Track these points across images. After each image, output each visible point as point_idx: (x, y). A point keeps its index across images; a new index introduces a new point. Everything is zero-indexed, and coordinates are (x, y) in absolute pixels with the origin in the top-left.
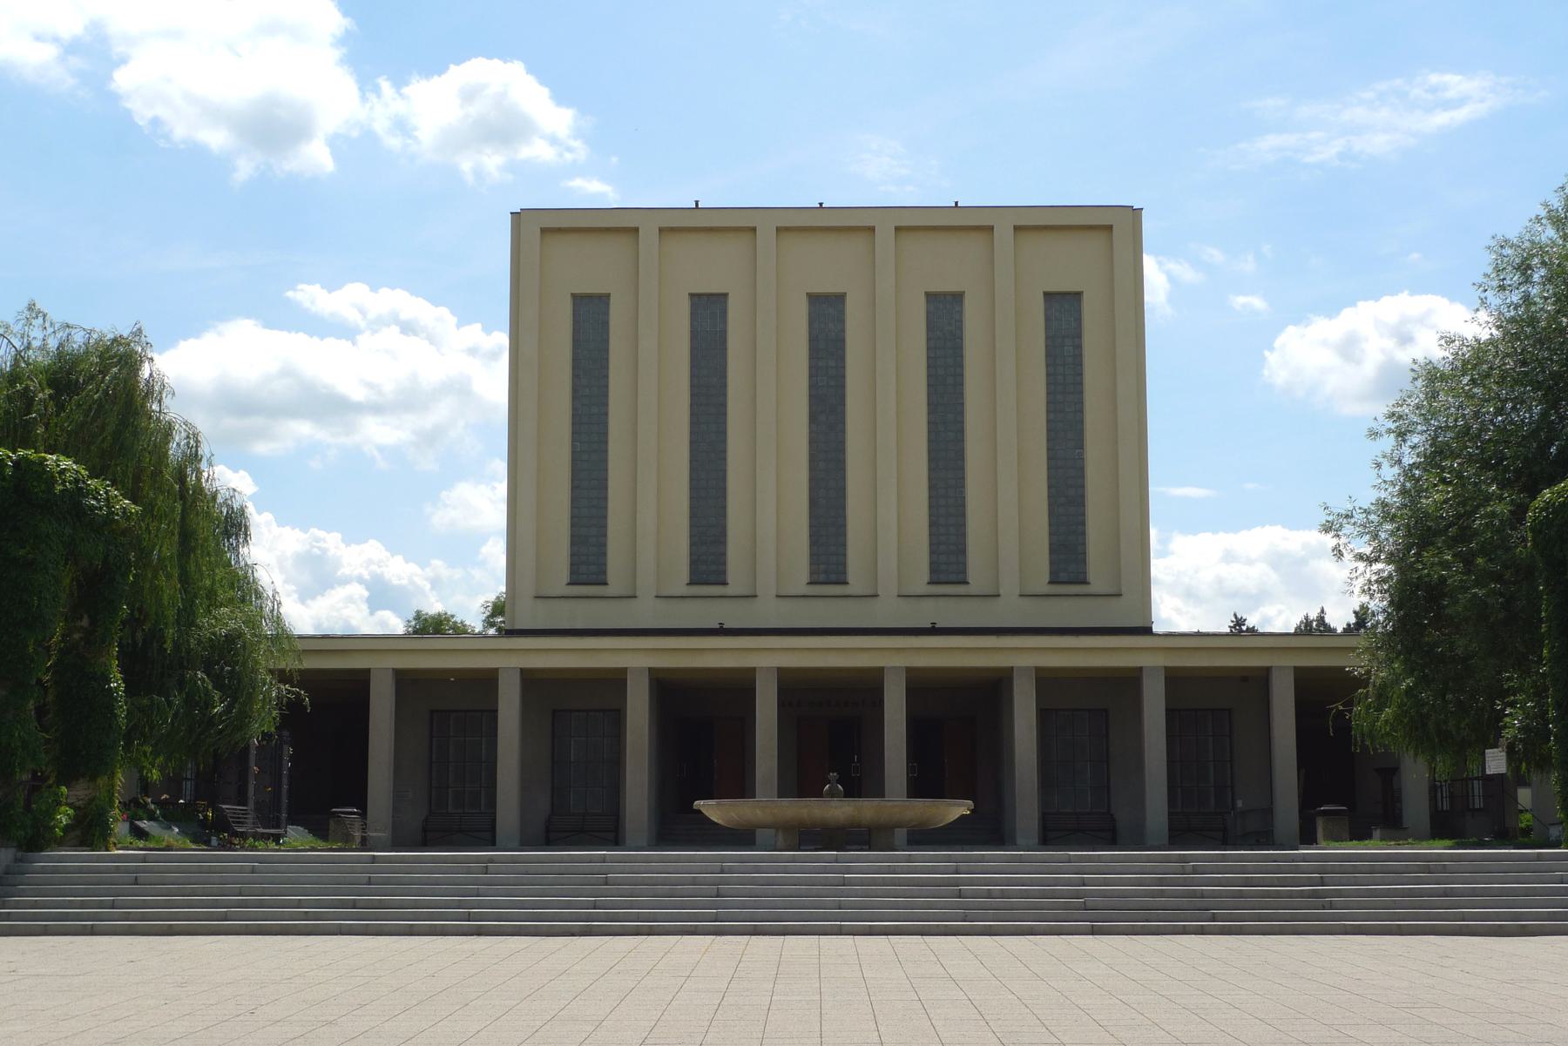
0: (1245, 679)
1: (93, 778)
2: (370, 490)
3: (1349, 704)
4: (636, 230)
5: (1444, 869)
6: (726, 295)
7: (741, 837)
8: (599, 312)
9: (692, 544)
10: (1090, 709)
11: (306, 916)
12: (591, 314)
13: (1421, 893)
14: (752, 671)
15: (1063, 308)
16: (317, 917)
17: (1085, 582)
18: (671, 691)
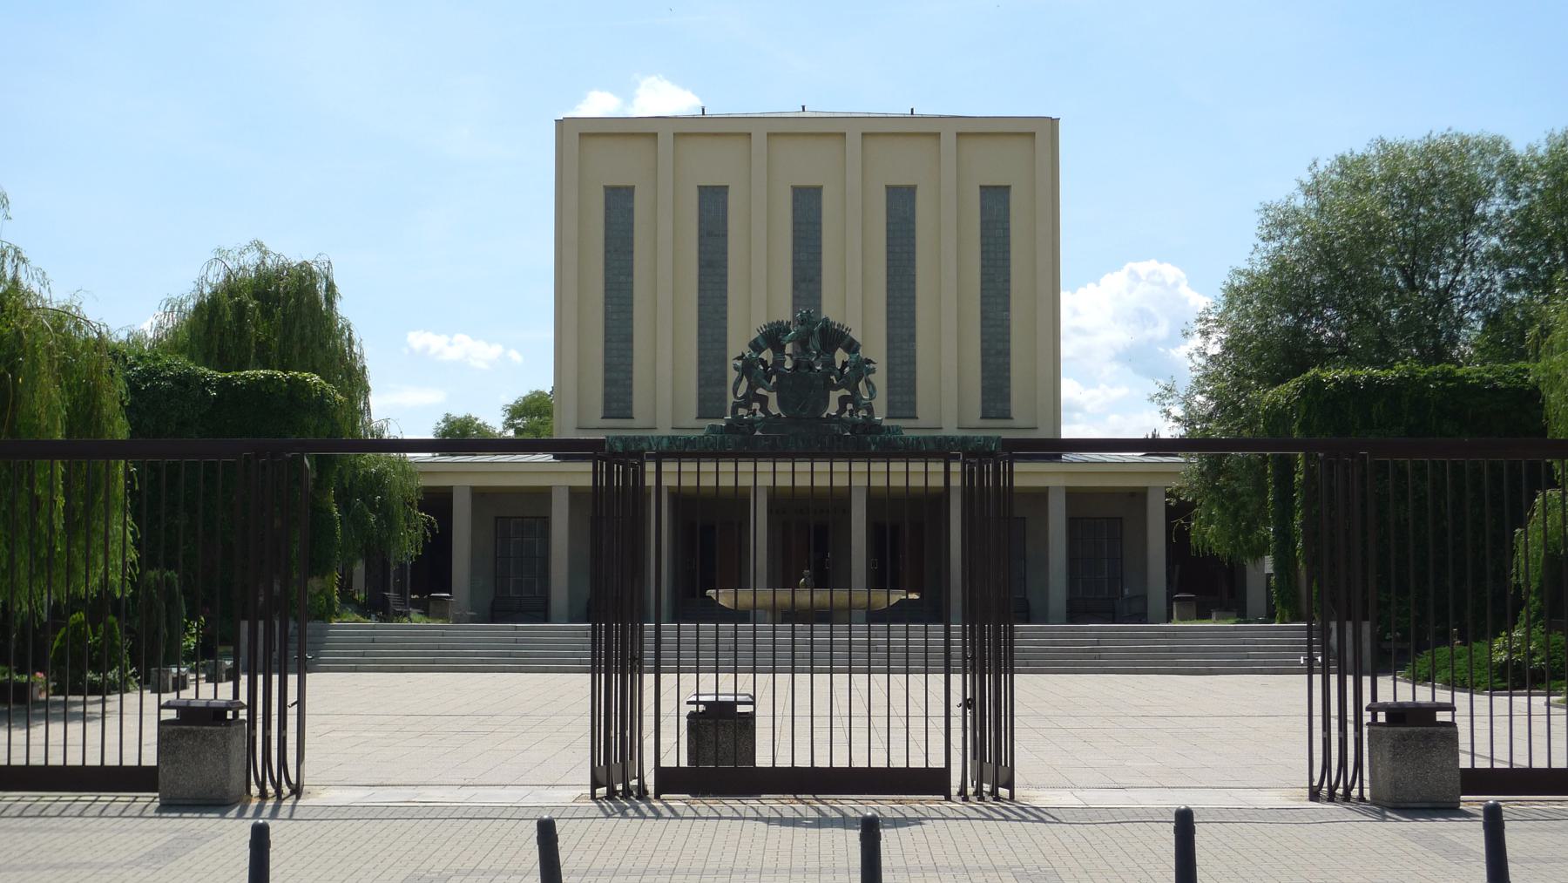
1: (323, 577)
2: (455, 350)
3: (1188, 519)
4: (656, 135)
5: (1175, 636)
7: (737, 615)
8: (616, 190)
9: (700, 386)
11: (482, 662)
12: (619, 201)
13: (1156, 650)
15: (995, 199)
16: (488, 662)
17: (1008, 417)
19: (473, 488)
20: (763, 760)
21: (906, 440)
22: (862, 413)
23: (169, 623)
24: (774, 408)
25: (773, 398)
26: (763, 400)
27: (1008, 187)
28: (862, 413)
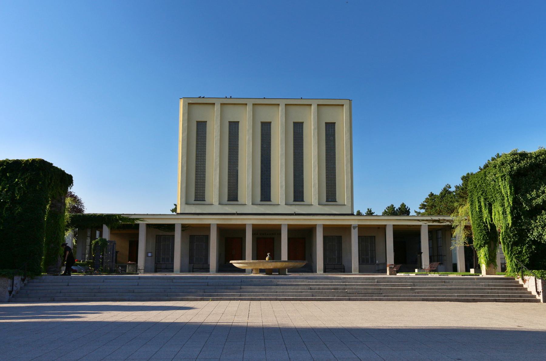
0: (379, 228)
6: (335, 123)
10: (336, 237)
14: (245, 225)
18: (222, 230)
27: (335, 123)
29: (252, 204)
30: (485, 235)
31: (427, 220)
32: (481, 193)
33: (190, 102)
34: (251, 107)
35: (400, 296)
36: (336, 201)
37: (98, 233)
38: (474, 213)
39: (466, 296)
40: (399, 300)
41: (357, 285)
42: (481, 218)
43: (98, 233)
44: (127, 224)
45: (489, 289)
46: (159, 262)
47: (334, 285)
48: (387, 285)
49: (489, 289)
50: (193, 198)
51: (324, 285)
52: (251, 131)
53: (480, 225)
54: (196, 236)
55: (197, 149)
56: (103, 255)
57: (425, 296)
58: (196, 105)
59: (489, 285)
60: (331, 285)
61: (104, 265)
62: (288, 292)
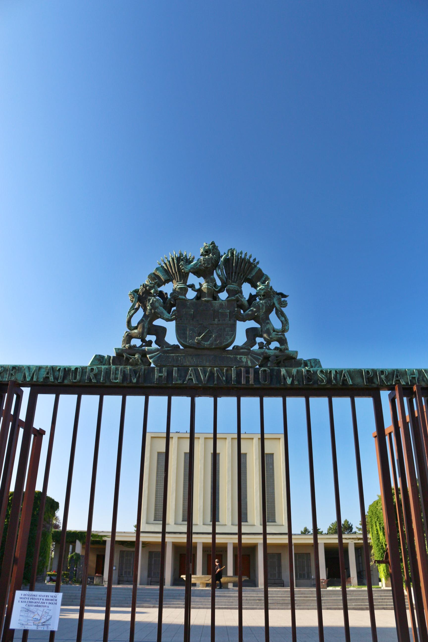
19: (325, 543)
20: (243, 588)
21: (328, 373)
22: (274, 345)
23: (64, 558)
24: (171, 338)
25: (171, 328)
26: (160, 332)
27: (273, 454)
28: (274, 345)
29: (203, 524)
30: (382, 554)
31: (353, 539)
32: (376, 518)
33: (153, 436)
34: (203, 440)
35: (310, 606)
36: (275, 522)
37: (71, 547)
38: (374, 535)
39: (361, 605)
40: (308, 609)
41: (277, 597)
42: (379, 539)
43: (71, 547)
44: (96, 541)
45: (380, 599)
46: (122, 575)
47: (259, 597)
48: (301, 597)
49: (380, 599)
50: (153, 519)
51: (251, 597)
52: (203, 461)
53: (378, 545)
54: (156, 553)
55: (157, 476)
56: (76, 568)
57: (329, 605)
58: (157, 439)
59: (381, 596)
60: (257, 597)
61: (77, 577)
62: (222, 602)
